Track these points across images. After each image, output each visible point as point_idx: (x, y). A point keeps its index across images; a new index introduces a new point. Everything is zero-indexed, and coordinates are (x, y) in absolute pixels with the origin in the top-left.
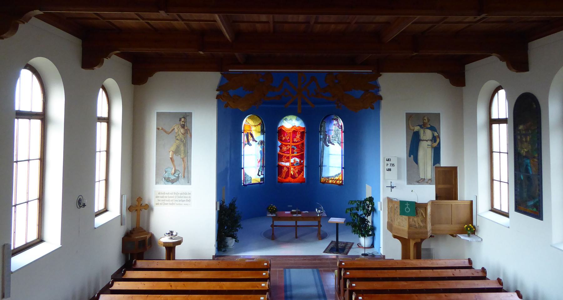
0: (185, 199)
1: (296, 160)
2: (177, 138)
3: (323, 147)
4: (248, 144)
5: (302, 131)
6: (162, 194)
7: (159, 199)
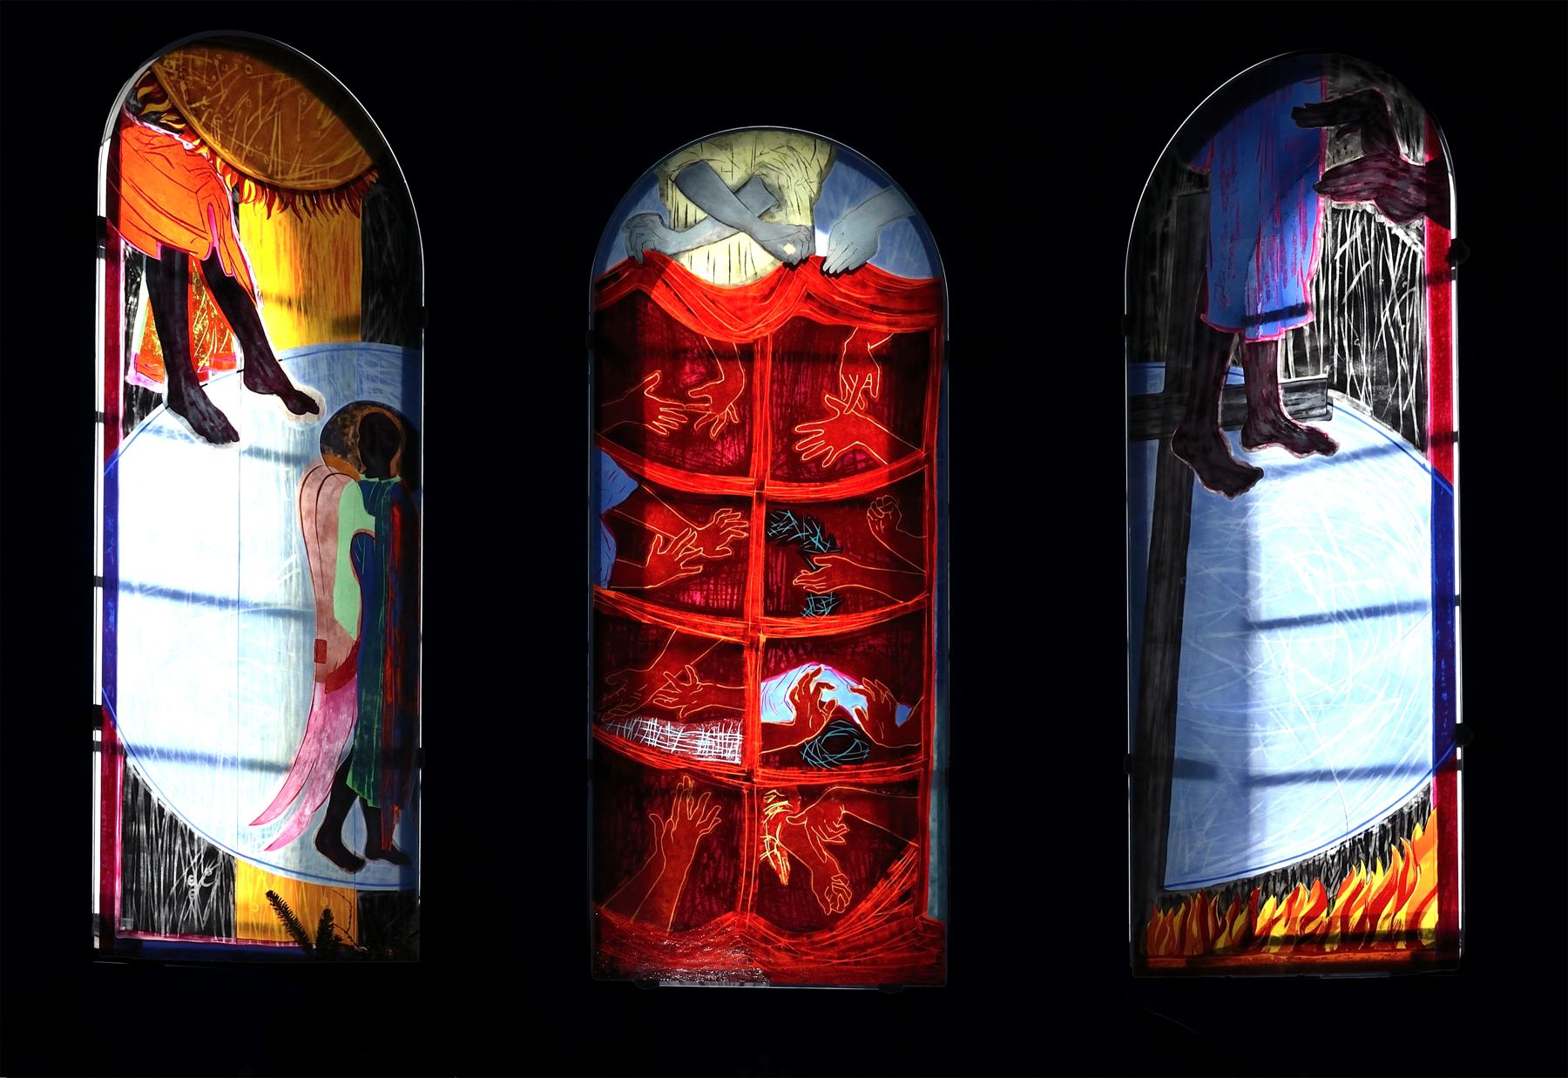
1: (826, 696)
4: (178, 404)
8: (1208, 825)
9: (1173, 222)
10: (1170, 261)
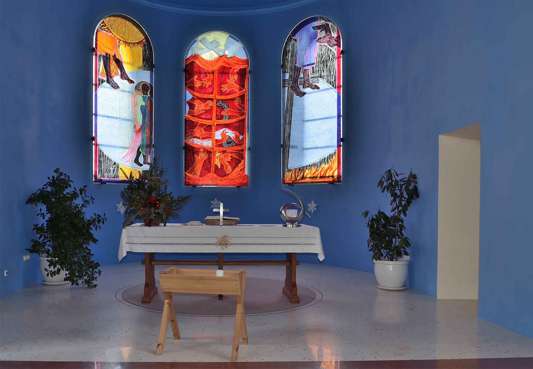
1: (227, 134)
3: (291, 100)
4: (108, 81)
5: (242, 67)
9: (290, 48)
10: (290, 55)
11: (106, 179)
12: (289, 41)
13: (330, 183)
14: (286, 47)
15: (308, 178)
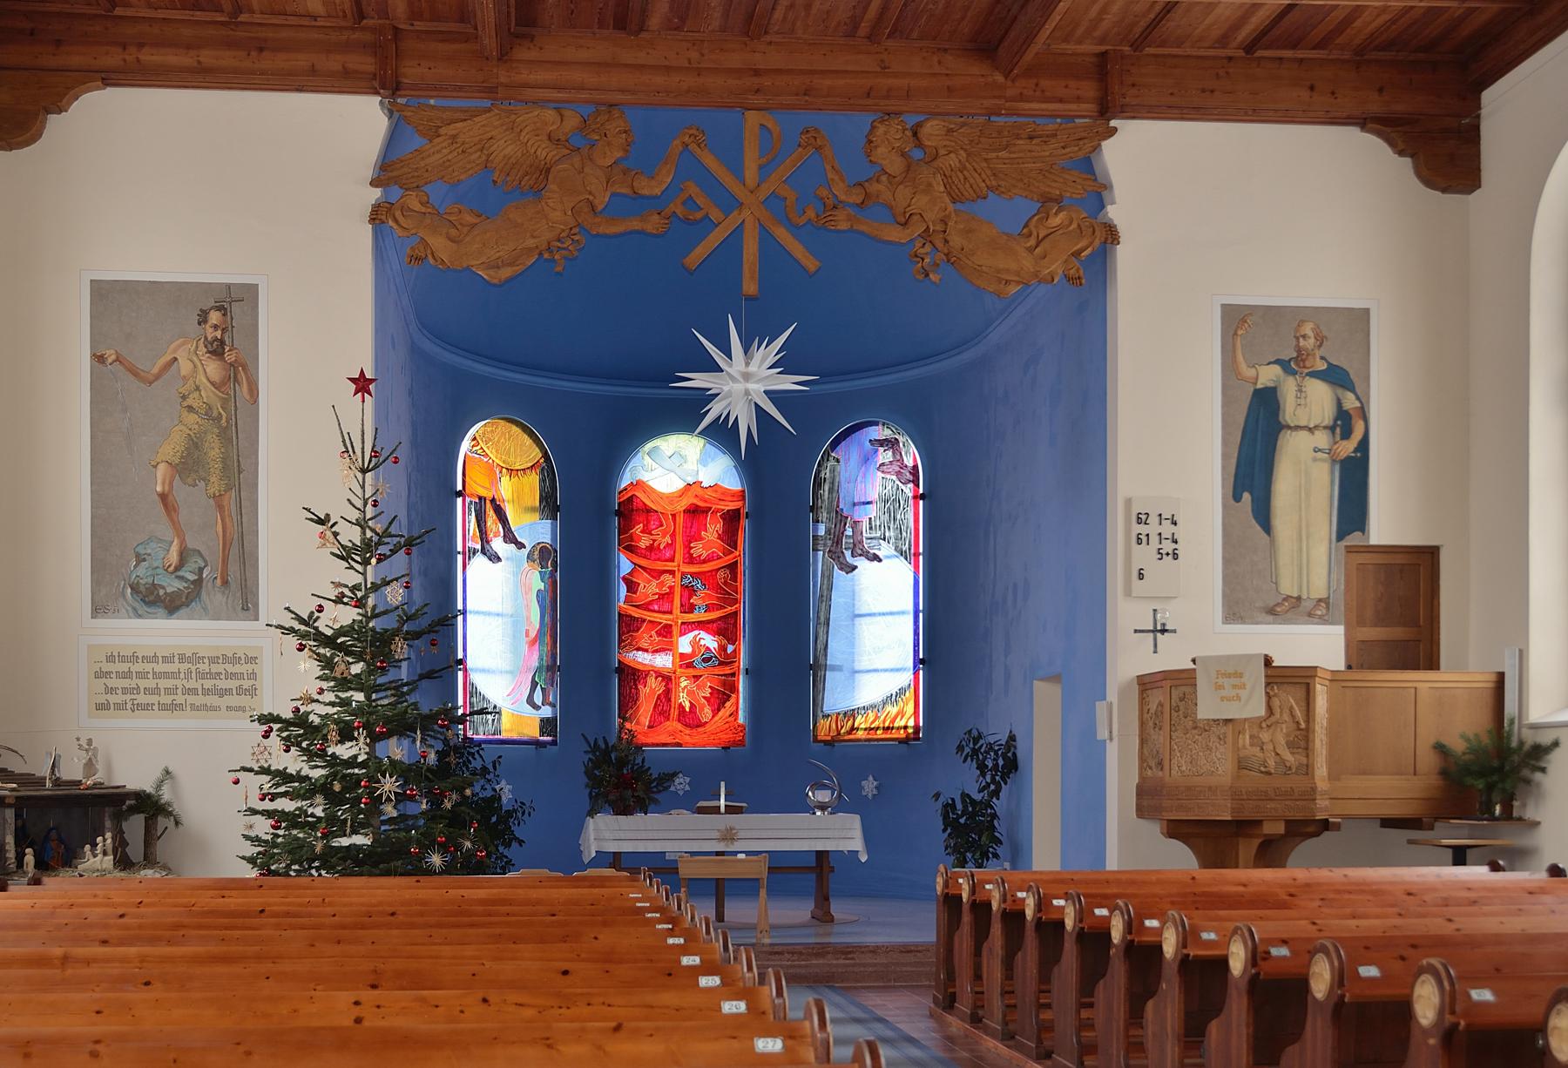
0: (232, 684)
1: (702, 642)
2: (189, 402)
3: (829, 577)
4: (484, 552)
5: (732, 506)
6: (123, 659)
7: (112, 683)
8: (839, 690)
9: (828, 474)
10: (827, 488)
11: (481, 737)
12: (826, 460)
13: (901, 741)
14: (818, 472)
15: (862, 729)
